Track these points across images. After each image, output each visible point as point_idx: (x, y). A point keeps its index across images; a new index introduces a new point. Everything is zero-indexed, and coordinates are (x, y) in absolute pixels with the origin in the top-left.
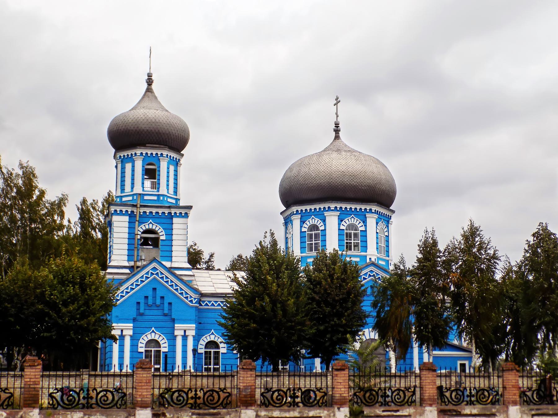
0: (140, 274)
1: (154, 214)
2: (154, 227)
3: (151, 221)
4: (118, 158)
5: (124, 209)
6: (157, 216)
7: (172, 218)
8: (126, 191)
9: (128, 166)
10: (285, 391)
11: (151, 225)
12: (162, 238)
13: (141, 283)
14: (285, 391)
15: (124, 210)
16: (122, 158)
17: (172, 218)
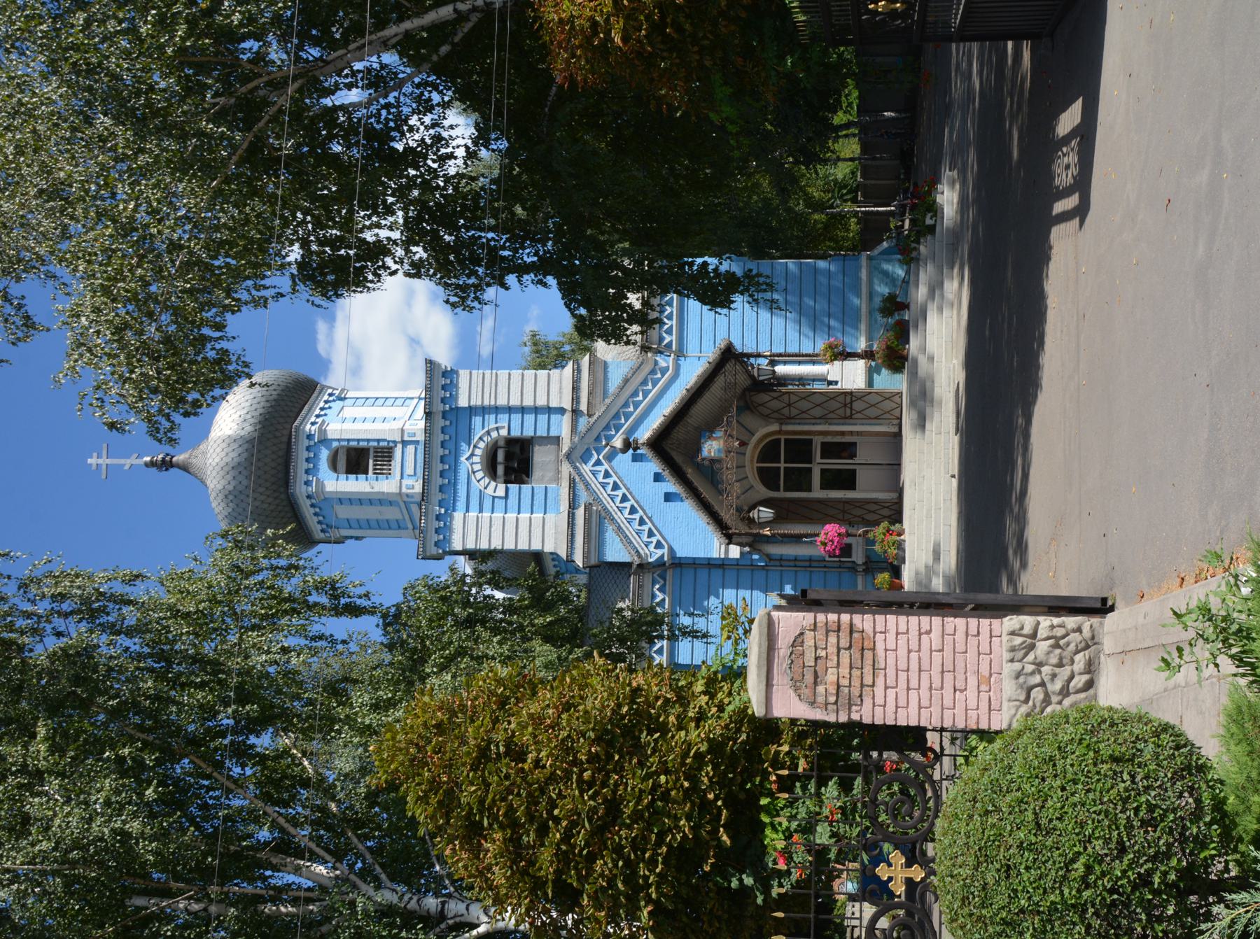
7: (458, 408)
8: (399, 517)
16: (324, 526)
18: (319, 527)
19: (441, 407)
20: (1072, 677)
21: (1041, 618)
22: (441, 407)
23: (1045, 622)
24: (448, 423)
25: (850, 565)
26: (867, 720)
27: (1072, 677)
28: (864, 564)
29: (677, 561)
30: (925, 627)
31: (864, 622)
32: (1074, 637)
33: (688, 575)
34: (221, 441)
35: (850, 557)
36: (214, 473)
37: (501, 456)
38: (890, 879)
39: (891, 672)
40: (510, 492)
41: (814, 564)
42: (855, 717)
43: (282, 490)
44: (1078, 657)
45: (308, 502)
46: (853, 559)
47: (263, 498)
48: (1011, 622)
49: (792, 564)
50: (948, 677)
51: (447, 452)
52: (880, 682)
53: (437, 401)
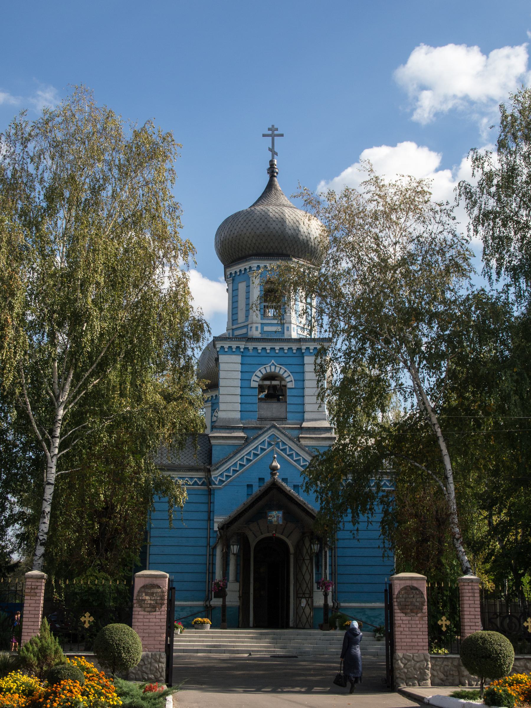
0: (246, 449)
1: (268, 351)
2: (277, 370)
3: (273, 361)
4: (229, 277)
5: (234, 345)
6: (281, 354)
7: (303, 357)
8: (240, 321)
9: (242, 286)
10: (518, 617)
11: (273, 368)
12: (289, 385)
13: (261, 453)
14: (518, 617)
15: (234, 346)
16: (234, 275)
17: (302, 356)
18: (233, 272)
19: (304, 347)
20: (147, 674)
21: (165, 664)
22: (304, 347)
23: (164, 666)
24: (294, 351)
25: (210, 597)
26: (134, 609)
27: (147, 674)
28: (210, 605)
29: (212, 492)
30: (163, 628)
31: (165, 608)
32: (159, 675)
33: (204, 499)
34: (282, 211)
35: (214, 597)
36: (264, 209)
37: (274, 383)
38: (85, 617)
39: (149, 617)
40: (253, 390)
41: (211, 575)
42: (135, 605)
43: (255, 252)
44: (153, 676)
45: (247, 267)
46: (214, 599)
47: (249, 242)
48: (164, 655)
49: (211, 562)
50: (147, 635)
51: (277, 351)
52: (146, 613)
53: (308, 345)
